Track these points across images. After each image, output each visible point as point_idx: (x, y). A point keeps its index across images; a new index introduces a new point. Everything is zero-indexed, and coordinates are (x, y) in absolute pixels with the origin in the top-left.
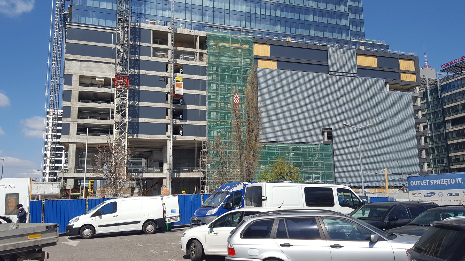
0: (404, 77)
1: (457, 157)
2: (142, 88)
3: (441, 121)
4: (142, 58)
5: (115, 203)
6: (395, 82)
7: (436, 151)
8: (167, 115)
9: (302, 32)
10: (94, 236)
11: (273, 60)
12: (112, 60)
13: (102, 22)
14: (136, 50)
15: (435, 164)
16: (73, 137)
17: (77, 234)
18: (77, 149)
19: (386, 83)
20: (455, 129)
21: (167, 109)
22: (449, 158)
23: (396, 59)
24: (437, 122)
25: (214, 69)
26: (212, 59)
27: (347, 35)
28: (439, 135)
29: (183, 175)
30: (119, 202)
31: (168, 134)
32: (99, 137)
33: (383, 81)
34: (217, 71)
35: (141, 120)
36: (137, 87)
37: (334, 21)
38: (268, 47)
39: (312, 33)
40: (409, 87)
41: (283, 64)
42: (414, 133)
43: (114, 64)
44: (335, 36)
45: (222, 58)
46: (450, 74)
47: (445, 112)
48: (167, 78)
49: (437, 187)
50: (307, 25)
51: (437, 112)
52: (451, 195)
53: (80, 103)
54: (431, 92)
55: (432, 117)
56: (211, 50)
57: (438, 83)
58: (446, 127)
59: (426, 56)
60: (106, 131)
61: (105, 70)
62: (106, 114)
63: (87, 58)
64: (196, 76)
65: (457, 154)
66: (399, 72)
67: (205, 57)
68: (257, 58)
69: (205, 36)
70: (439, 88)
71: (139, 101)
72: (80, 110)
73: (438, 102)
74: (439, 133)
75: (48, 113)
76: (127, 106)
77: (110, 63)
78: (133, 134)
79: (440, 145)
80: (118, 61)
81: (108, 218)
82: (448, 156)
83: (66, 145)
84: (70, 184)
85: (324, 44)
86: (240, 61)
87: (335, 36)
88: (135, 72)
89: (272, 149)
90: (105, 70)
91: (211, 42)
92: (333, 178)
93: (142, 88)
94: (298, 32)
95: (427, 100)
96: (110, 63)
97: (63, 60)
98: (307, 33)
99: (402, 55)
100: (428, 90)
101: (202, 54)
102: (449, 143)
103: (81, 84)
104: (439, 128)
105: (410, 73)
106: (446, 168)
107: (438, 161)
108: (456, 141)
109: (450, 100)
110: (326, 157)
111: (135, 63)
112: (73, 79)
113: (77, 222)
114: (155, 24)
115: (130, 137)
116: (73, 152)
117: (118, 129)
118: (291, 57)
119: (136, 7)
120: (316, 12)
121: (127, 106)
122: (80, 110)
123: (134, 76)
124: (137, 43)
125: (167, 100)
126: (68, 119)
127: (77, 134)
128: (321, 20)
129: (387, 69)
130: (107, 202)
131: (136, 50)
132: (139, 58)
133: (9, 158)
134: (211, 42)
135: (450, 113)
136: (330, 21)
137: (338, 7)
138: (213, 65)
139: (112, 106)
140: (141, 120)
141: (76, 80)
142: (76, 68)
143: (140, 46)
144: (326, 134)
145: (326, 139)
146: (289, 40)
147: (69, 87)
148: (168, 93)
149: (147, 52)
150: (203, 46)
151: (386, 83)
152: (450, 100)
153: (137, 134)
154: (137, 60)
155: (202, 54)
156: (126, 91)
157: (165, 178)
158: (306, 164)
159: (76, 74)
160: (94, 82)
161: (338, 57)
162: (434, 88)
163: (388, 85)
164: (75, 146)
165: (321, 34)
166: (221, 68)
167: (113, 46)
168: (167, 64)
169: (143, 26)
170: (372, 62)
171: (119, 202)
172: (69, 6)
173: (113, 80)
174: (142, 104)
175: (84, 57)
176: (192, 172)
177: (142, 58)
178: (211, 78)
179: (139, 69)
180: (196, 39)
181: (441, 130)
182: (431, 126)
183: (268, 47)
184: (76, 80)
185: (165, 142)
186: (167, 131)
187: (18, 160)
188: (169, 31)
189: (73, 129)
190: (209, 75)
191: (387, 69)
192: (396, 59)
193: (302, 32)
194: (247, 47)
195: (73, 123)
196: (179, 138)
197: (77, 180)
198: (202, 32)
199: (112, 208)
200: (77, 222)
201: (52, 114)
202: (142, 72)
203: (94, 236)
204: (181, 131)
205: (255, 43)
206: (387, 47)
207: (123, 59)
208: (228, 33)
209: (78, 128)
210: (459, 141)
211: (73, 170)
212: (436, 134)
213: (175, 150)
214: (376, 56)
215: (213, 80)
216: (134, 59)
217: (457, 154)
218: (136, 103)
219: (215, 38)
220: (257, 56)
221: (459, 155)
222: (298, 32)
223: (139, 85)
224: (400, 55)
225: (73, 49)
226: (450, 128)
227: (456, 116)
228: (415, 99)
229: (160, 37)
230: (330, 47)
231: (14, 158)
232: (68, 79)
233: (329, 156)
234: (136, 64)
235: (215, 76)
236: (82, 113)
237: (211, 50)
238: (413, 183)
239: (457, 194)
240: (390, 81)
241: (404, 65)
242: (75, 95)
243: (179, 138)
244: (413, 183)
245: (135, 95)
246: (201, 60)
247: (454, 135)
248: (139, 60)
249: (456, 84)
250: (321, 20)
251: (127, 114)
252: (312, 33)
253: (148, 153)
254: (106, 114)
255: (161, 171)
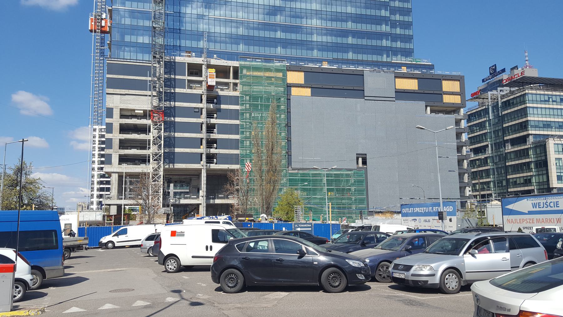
0: (447, 99)
1: (515, 180)
2: (178, 119)
3: (501, 140)
4: (178, 90)
5: (126, 229)
6: (436, 104)
7: (496, 173)
8: (201, 145)
9: (340, 56)
10: (114, 247)
11: (307, 87)
12: (149, 93)
13: (140, 56)
14: (170, 83)
15: (495, 186)
16: (115, 167)
17: (105, 246)
18: (119, 176)
19: (426, 106)
20: (513, 150)
21: (202, 139)
22: (508, 180)
23: (439, 79)
24: (498, 141)
25: (248, 98)
26: (246, 88)
27: (388, 56)
28: (499, 156)
29: (217, 201)
30: (129, 228)
31: (202, 162)
32: (139, 166)
33: (423, 104)
34: (250, 101)
35: (177, 150)
36: (172, 119)
37: (374, 43)
38: (302, 74)
39: (350, 56)
40: (453, 109)
41: (317, 91)
42: (454, 157)
43: (150, 96)
44: (375, 58)
45: (255, 87)
46: (513, 89)
47: (505, 131)
48: (202, 109)
49: (418, 214)
50: (345, 48)
51: (498, 131)
52: (425, 221)
53: (121, 135)
54: (493, 107)
55: (493, 136)
56: (244, 80)
57: (499, 99)
58: (505, 147)
59: (526, 54)
60: (144, 160)
61: (142, 102)
62: (143, 145)
63: (126, 92)
64: (230, 106)
65: (514, 176)
66: (441, 94)
67: (239, 87)
68: (289, 86)
69: (238, 66)
70: (500, 105)
71: (175, 132)
72: (121, 141)
73: (499, 120)
74: (499, 153)
75: (95, 130)
76: (163, 139)
77: (147, 96)
78: (169, 163)
79: (500, 166)
80: (155, 93)
81: (122, 238)
82: (507, 179)
83: (109, 175)
84: (113, 211)
85: (360, 68)
86: (272, 89)
87: (375, 58)
88: (170, 104)
89: (303, 175)
90: (142, 102)
91: (245, 72)
92: (365, 203)
93: (178, 119)
94: (335, 55)
95: (489, 117)
96: (147, 96)
97: (104, 94)
98: (345, 56)
99: (446, 76)
100: (490, 107)
101: (235, 85)
102: (507, 164)
103: (122, 116)
104: (499, 148)
105: (454, 95)
106: (505, 191)
107: (498, 183)
108: (513, 163)
109: (516, 116)
110: (359, 182)
111: (170, 96)
112: (114, 112)
113: (104, 240)
114: (190, 56)
115: (167, 167)
116: (116, 180)
117: (155, 160)
118: (326, 84)
119: (172, 40)
120: (356, 34)
121: (163, 139)
122: (121, 141)
123: (170, 108)
124: (172, 76)
125: (202, 130)
126: (111, 150)
127: (119, 164)
128: (360, 42)
129: (429, 91)
130: (122, 228)
131: (170, 83)
132: (174, 90)
133: (54, 174)
134: (245, 72)
135: (509, 133)
136: (370, 42)
137: (378, 27)
138: (246, 95)
139: (150, 137)
140: (177, 150)
141: (116, 113)
142: (117, 101)
143: (175, 79)
144: (360, 160)
145: (360, 164)
146: (325, 65)
147: (111, 119)
148: (202, 123)
149: (182, 84)
150: (236, 76)
151: (426, 106)
152: (509, 118)
153: (174, 163)
154: (172, 93)
155: (235, 85)
156: (161, 125)
157: (201, 204)
158: (337, 190)
159: (116, 107)
160: (134, 114)
161: (374, 81)
162: (495, 104)
163: (429, 108)
164: (117, 175)
165: (360, 57)
166: (254, 98)
167: (150, 79)
168: (201, 95)
169: (178, 59)
170: (412, 85)
171: (129, 228)
172: (109, 42)
173: (150, 111)
174: (177, 135)
175: (124, 90)
176: (228, 198)
177: (178, 90)
178: (244, 107)
179: (175, 102)
180: (230, 69)
181: (501, 150)
182: (492, 145)
183: (302, 74)
184: (116, 113)
185: (200, 170)
186: (201, 160)
187: (64, 177)
188: (203, 63)
189: (115, 159)
190: (242, 105)
191: (429, 91)
192: (439, 79)
193: (340, 56)
194: (280, 75)
195: (115, 153)
196: (213, 166)
197: (119, 207)
198: (235, 62)
199: (125, 232)
200: (104, 240)
201: (97, 131)
202: (178, 104)
203: (114, 247)
204: (215, 160)
205: (288, 70)
206: (431, 67)
207: (160, 92)
208: (262, 62)
209: (119, 158)
210: (517, 162)
211: (116, 197)
212: (496, 154)
213: (208, 176)
214: (417, 78)
215: (246, 109)
216: (170, 92)
217: (514, 176)
218: (172, 134)
219: (248, 68)
220: (290, 84)
221: (516, 178)
222: (335, 55)
223: (174, 117)
224: (443, 76)
225: (112, 84)
226: (509, 148)
227: (515, 136)
228: (458, 122)
229: (195, 70)
230: (367, 70)
231: (59, 175)
232: (110, 113)
233: (362, 183)
234: (171, 97)
235: (248, 106)
236: (123, 144)
237: (244, 80)
238: (404, 211)
239: (429, 221)
240: (432, 104)
241: (447, 86)
242: (116, 127)
243: (213, 166)
244: (404, 211)
245: (170, 126)
246: (235, 90)
247: (513, 156)
248: (175, 93)
249: (515, 101)
250: (360, 42)
251: (162, 147)
252: (350, 56)
253: (188, 180)
254: (143, 145)
255: (198, 197)
